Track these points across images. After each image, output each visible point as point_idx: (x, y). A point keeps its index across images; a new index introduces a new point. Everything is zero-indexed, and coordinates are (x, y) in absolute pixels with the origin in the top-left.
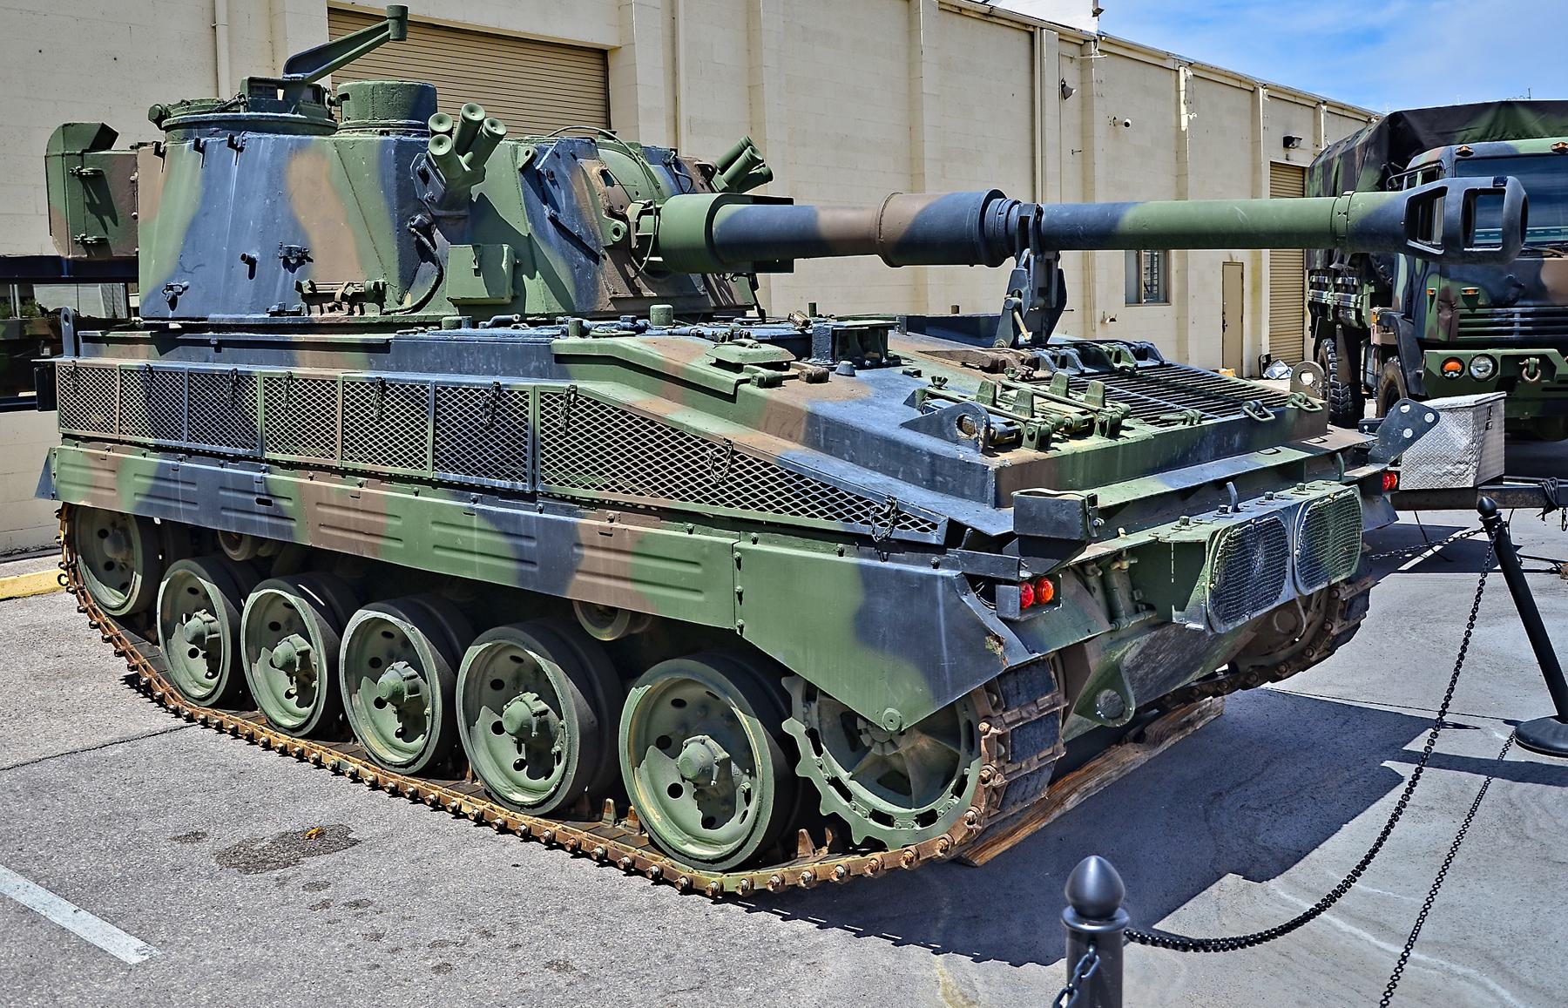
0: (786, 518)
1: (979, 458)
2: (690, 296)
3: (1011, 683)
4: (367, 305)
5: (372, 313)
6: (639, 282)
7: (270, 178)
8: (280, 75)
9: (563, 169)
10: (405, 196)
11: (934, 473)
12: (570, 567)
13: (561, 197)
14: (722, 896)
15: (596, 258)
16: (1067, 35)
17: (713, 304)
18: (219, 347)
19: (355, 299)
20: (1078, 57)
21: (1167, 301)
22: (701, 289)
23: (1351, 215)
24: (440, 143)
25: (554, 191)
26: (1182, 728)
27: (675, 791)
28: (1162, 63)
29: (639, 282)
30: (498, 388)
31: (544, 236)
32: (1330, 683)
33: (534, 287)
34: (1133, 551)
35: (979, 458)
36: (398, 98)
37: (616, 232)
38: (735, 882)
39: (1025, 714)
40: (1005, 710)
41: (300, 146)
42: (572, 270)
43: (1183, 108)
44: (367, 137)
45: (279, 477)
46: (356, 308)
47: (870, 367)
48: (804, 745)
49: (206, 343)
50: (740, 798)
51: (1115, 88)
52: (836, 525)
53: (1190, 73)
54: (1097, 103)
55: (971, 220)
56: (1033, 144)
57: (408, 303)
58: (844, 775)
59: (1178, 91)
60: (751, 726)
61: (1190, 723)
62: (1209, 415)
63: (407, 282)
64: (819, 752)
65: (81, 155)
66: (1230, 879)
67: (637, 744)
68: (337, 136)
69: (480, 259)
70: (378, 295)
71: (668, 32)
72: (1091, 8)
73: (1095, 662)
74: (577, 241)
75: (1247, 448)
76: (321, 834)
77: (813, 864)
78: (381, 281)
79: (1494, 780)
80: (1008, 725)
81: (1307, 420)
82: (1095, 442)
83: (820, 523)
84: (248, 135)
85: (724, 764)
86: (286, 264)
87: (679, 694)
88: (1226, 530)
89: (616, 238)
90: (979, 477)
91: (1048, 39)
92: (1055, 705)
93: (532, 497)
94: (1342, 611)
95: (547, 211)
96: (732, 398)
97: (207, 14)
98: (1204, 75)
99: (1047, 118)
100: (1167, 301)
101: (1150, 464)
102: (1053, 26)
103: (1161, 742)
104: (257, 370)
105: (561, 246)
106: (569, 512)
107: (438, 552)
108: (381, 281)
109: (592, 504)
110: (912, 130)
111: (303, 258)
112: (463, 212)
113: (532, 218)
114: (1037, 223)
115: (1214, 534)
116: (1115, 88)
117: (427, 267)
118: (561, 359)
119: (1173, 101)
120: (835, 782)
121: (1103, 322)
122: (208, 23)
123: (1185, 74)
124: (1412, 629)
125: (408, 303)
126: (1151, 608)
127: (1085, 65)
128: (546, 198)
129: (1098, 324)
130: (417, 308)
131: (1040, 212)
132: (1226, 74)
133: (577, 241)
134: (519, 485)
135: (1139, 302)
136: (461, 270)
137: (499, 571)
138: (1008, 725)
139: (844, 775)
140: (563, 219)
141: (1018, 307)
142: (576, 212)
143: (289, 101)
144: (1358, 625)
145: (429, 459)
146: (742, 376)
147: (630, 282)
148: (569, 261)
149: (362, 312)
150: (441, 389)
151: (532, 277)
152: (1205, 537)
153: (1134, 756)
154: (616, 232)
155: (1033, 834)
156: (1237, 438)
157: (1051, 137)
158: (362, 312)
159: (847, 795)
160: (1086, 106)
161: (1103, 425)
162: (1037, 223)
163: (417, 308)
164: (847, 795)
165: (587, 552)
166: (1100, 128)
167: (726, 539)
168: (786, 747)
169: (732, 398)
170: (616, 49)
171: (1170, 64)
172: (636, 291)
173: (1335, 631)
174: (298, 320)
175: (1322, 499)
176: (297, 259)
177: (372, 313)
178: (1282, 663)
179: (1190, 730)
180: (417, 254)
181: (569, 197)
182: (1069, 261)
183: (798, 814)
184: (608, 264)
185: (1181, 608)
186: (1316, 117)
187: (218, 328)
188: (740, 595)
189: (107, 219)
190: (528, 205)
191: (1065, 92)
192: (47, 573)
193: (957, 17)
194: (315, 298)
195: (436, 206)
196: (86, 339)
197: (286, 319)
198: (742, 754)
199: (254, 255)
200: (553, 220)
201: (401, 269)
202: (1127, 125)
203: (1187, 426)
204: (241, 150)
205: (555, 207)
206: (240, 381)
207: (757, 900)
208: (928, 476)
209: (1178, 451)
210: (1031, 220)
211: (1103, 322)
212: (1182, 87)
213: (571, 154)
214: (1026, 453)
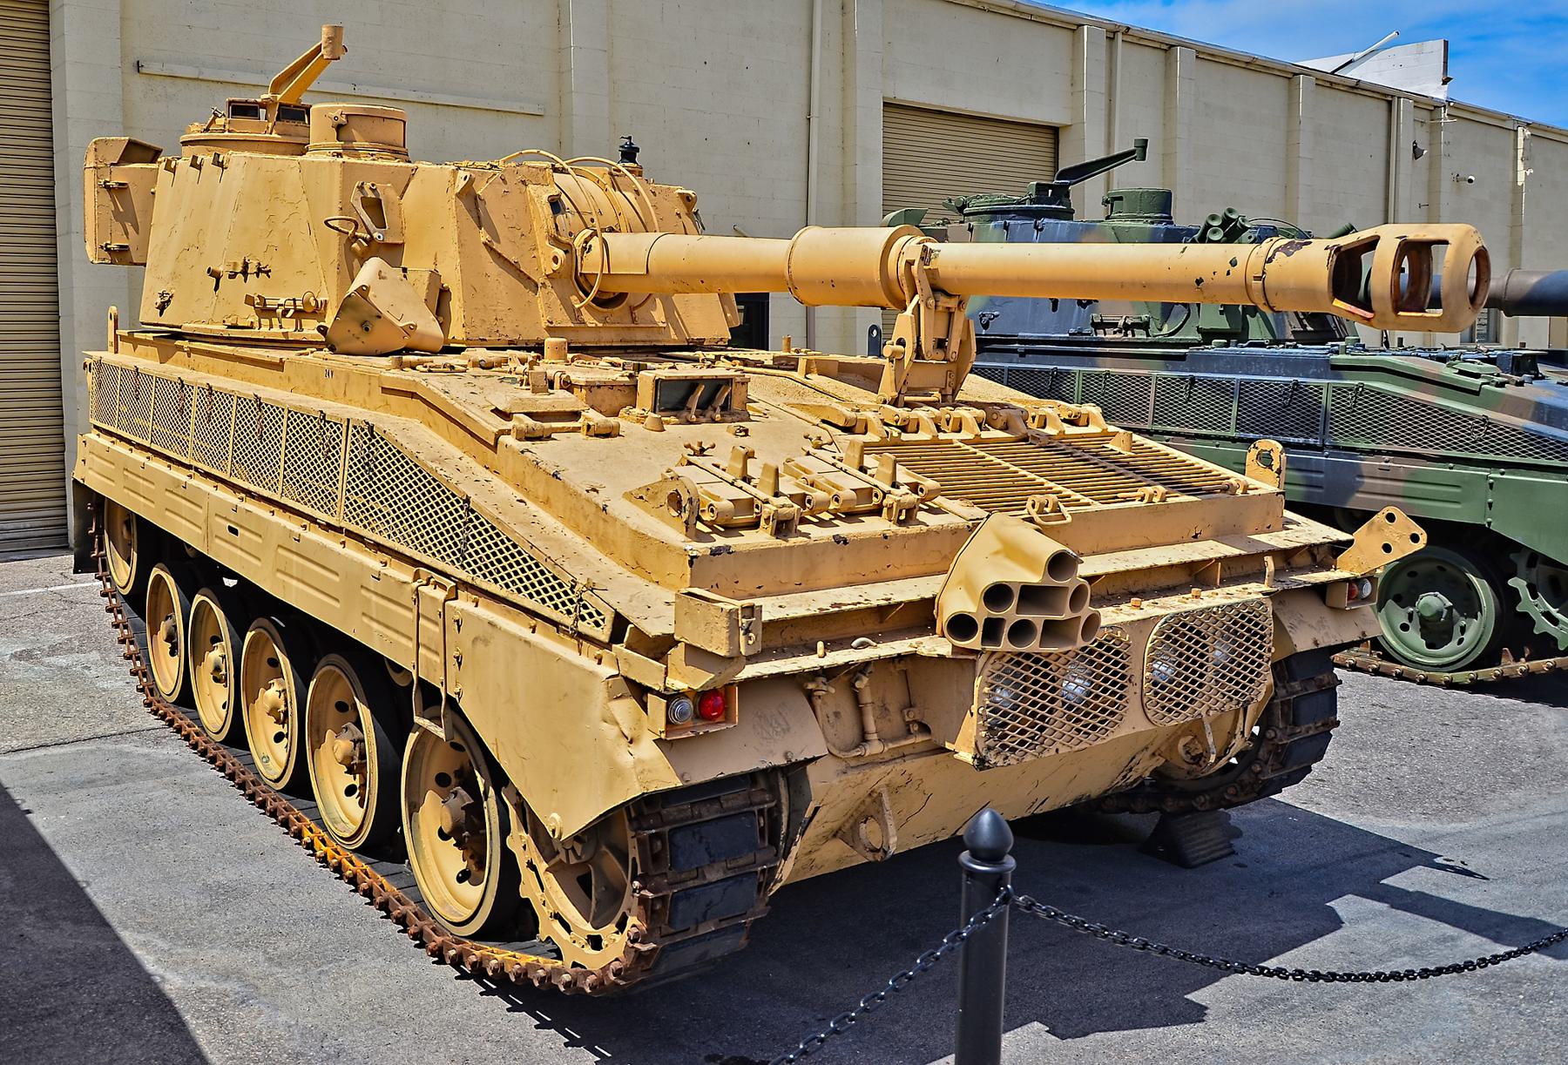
0: (1530, 460)
5: (1140, 335)
12: (1353, 489)
14: (1450, 685)
18: (1022, 355)
19: (1126, 327)
27: (1405, 627)
28: (1502, 124)
30: (1297, 383)
37: (555, 259)
38: (1463, 677)
43: (1520, 165)
44: (1141, 225)
48: (1524, 593)
49: (1015, 351)
50: (1457, 629)
51: (1459, 150)
54: (1445, 162)
57: (1165, 330)
58: (1554, 611)
60: (1481, 586)
64: (1534, 596)
68: (308, 157)
70: (1145, 326)
72: (1441, 77)
83: (1556, 463)
85: (1449, 609)
87: (1414, 569)
89: (556, 267)
93: (1321, 449)
95: (484, 236)
96: (1477, 393)
98: (1540, 133)
99: (1402, 177)
104: (1155, 373)
106: (1351, 457)
109: (1372, 452)
116: (1459, 150)
118: (1335, 368)
120: (1548, 615)
122: (805, 115)
123: (1523, 133)
126: (925, 729)
127: (1434, 128)
134: (1311, 441)
139: (1554, 611)
145: (1233, 422)
146: (508, 425)
147: (575, 314)
150: (1242, 384)
154: (555, 259)
157: (1403, 193)
159: (1555, 621)
160: (1434, 166)
161: (890, 508)
164: (1555, 621)
166: (1446, 185)
167: (1482, 472)
168: (1508, 598)
169: (1477, 393)
171: (1509, 125)
172: (1304, 326)
177: (1140, 335)
183: (1514, 632)
186: (1169, 65)
187: (1022, 342)
188: (1490, 505)
191: (1417, 153)
194: (265, 311)
197: (235, 333)
198: (1469, 606)
203: (1143, 504)
205: (492, 231)
207: (1476, 687)
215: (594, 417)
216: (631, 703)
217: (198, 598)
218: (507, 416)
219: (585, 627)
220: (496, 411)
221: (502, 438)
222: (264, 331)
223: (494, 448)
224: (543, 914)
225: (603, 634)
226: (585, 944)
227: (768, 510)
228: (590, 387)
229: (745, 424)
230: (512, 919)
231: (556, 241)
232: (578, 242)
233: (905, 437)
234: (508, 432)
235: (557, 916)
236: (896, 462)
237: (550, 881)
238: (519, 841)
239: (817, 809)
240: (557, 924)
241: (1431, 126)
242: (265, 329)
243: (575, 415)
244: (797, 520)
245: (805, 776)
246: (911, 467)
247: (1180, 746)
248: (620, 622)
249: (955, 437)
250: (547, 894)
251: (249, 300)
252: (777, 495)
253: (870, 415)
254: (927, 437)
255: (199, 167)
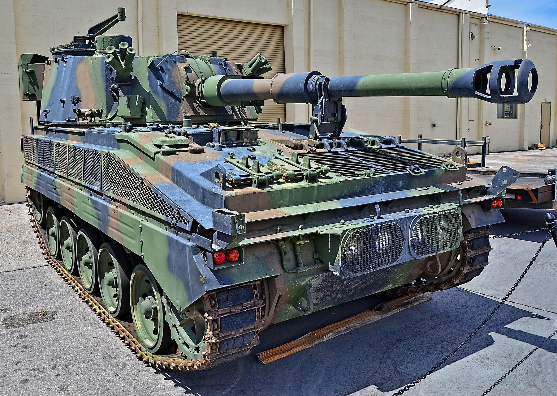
1: (220, 191)
2: (226, 115)
3: (224, 296)
4: (96, 118)
5: (97, 121)
6: (199, 109)
7: (72, 71)
8: (86, 35)
9: (169, 67)
10: (108, 81)
11: (204, 197)
13: (166, 77)
15: (180, 101)
16: (473, 15)
17: (235, 118)
19: (92, 115)
20: (479, 23)
21: (516, 117)
22: (230, 113)
23: (450, 80)
24: (109, 57)
25: (163, 75)
26: (403, 305)
28: (516, 25)
29: (199, 109)
31: (156, 93)
32: (492, 288)
33: (150, 113)
34: (306, 236)
35: (220, 191)
36: (113, 41)
37: (187, 90)
39: (233, 310)
40: (219, 308)
41: (81, 60)
42: (168, 105)
43: (525, 43)
45: (58, 181)
46: (93, 119)
47: (236, 146)
52: (163, 217)
53: (528, 29)
54: (486, 41)
55: (302, 85)
56: (458, 57)
57: (109, 117)
59: (523, 36)
61: (408, 303)
62: (388, 172)
63: (109, 110)
65: (27, 65)
66: (372, 388)
67: (135, 296)
69: (129, 101)
70: (99, 114)
71: (307, 19)
73: (281, 286)
74: (171, 94)
75: (407, 187)
76: (45, 314)
77: (170, 361)
78: (100, 109)
79: (540, 350)
80: (219, 315)
81: (451, 175)
82: (303, 184)
84: (69, 57)
86: (74, 103)
88: (354, 229)
90: (220, 201)
91: (465, 18)
92: (254, 306)
94: (469, 263)
95: (159, 82)
97: (136, 18)
98: (534, 29)
100: (516, 117)
101: (337, 195)
102: (467, 12)
103: (389, 311)
105: (164, 96)
107: (84, 213)
108: (100, 109)
110: (406, 52)
111: (79, 100)
112: (128, 83)
113: (151, 85)
114: (326, 85)
115: (344, 232)
117: (116, 103)
118: (119, 141)
119: (521, 39)
121: (486, 125)
122: (136, 21)
124: (550, 264)
125: (109, 117)
126: (322, 262)
127: (482, 27)
128: (159, 77)
129: (484, 126)
130: (112, 119)
131: (327, 80)
132: (548, 29)
133: (171, 94)
135: (503, 117)
136: (123, 106)
137: (93, 221)
138: (219, 315)
140: (165, 85)
141: (316, 122)
142: (172, 83)
143: (82, 46)
144: (483, 268)
146: (158, 150)
148: (167, 102)
149: (95, 120)
151: (149, 108)
152: (340, 233)
153: (374, 317)
154: (187, 90)
155: (302, 351)
156: (401, 183)
158: (95, 120)
161: (306, 176)
162: (326, 85)
163: (112, 119)
165: (111, 218)
170: (287, 25)
171: (520, 26)
173: (465, 271)
174: (73, 123)
175: (429, 214)
176: (76, 101)
178: (443, 283)
179: (409, 306)
180: (112, 99)
181: (170, 77)
182: (346, 101)
184: (185, 103)
185: (332, 264)
189: (35, 87)
190: (150, 81)
191: (472, 37)
192: (24, 209)
193: (426, 10)
194: (80, 115)
195: (121, 80)
196: (36, 128)
197: (70, 123)
199: (65, 99)
200: (161, 86)
201: (107, 105)
202: (499, 49)
204: (66, 62)
205: (162, 81)
206: (51, 143)
208: (202, 198)
209: (358, 189)
210: (323, 84)
211: (486, 125)
212: (525, 34)
213: (173, 60)
214: (253, 189)
215: (195, 146)
216: (201, 256)
217: (80, 233)
218: (159, 146)
219: (181, 225)
220: (156, 145)
221: (157, 155)
222: (80, 122)
223: (154, 159)
224: (179, 343)
225: (188, 228)
226: (193, 354)
227: (254, 178)
228: (194, 135)
229: (254, 147)
230: (168, 347)
231: (187, 83)
232: (197, 84)
233: (318, 151)
234: (159, 152)
235: (185, 343)
236: (310, 160)
237: (181, 329)
238: (170, 315)
239: (280, 296)
240: (185, 346)
241: (480, 26)
242: (81, 121)
243: (187, 146)
244: (267, 182)
245: (274, 281)
246: (317, 161)
247: (428, 266)
248: (195, 223)
249: (340, 150)
250: (180, 335)
251: (75, 111)
252: (259, 172)
253: (303, 143)
254: (326, 150)
255: (58, 62)
